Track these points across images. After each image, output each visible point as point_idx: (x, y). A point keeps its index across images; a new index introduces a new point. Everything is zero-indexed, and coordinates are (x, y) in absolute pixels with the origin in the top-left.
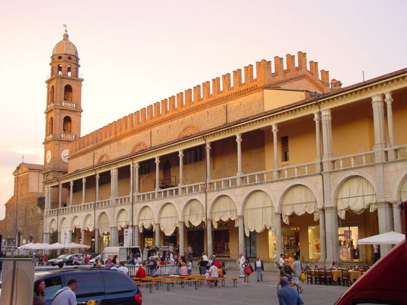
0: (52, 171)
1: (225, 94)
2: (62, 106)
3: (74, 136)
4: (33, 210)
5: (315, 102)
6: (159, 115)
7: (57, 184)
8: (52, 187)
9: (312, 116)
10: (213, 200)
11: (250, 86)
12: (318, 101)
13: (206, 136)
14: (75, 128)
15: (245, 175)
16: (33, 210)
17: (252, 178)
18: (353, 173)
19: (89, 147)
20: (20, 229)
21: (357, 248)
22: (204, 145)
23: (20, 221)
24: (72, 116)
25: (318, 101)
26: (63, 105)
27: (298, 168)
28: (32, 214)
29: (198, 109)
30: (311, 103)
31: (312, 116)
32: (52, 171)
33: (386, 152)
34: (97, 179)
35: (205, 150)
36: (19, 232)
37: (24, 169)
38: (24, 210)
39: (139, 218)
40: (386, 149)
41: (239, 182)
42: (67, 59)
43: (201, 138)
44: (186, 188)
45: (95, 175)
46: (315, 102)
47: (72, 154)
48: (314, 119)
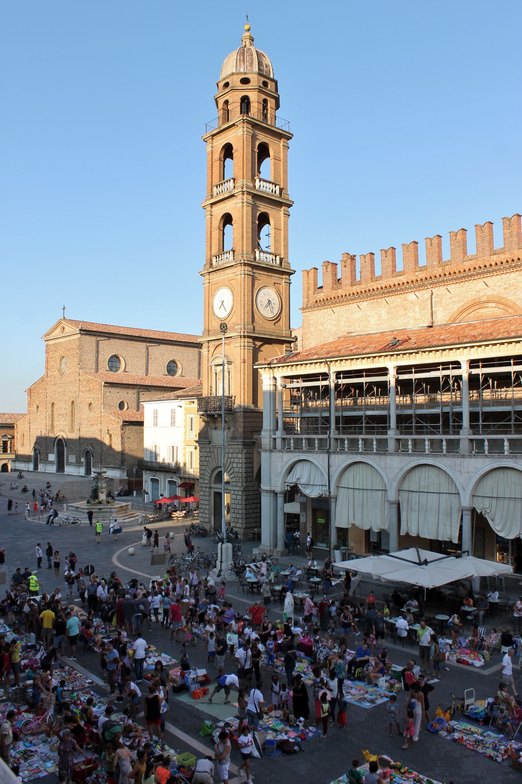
6: (373, 278)
23: (62, 422)
30: (404, 352)
38: (70, 403)
42: (262, 85)
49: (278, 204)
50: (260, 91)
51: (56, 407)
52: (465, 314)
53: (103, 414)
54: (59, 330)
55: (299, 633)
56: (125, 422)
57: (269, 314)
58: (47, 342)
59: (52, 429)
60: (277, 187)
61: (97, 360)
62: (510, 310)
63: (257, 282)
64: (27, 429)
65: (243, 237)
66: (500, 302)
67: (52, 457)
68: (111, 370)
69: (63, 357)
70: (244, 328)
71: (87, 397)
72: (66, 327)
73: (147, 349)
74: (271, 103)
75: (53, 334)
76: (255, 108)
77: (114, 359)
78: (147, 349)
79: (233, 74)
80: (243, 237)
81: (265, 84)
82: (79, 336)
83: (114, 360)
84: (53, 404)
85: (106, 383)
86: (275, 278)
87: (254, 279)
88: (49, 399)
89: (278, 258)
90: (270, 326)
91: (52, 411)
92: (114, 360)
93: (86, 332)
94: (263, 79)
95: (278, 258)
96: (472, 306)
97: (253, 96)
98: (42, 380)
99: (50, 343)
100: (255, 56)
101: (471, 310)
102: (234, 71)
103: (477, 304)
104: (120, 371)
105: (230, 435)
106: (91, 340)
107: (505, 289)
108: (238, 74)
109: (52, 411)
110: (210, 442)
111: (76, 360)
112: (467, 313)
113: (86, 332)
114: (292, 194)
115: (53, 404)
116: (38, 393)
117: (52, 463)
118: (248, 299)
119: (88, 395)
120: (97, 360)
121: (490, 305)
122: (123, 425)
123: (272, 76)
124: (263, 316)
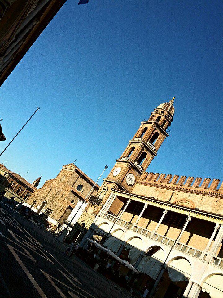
0: (115, 183)
2: (147, 143)
4: (63, 195)
5: (189, 210)
7: (127, 197)
8: (118, 197)
9: (215, 224)
15: (219, 258)
16: (63, 195)
19: (169, 185)
21: (30, 221)
22: (128, 199)
27: (190, 248)
29: (165, 188)
31: (215, 224)
32: (115, 183)
33: (206, 255)
35: (185, 221)
36: (45, 202)
37: (72, 167)
38: (57, 192)
39: (206, 280)
40: (207, 253)
44: (219, 260)
46: (189, 210)
47: (144, 181)
48: (144, 206)
49: (151, 153)
50: (165, 117)
51: (51, 191)
52: (179, 202)
53: (64, 200)
54: (69, 166)
55: (53, 225)
56: (69, 206)
57: (130, 183)
58: (63, 168)
59: (45, 198)
60: (154, 148)
61: (75, 183)
62: (192, 206)
63: (130, 171)
64: (37, 193)
65: (134, 155)
66: (191, 202)
67: (39, 207)
68: (77, 189)
69: (65, 176)
70: (118, 181)
71: (63, 192)
72: (72, 166)
73: (94, 190)
74: (167, 123)
75: (67, 167)
76: (160, 121)
77: (81, 186)
78: (94, 190)
79: (160, 108)
80: (134, 155)
81: (169, 116)
82: (74, 171)
83: (80, 187)
84: (51, 189)
85: (72, 190)
86: (137, 174)
87: (130, 169)
88: (51, 187)
89: (142, 168)
90: (127, 187)
91: (50, 191)
92: (80, 187)
93: (77, 171)
94: (168, 114)
95: (142, 168)
96: (183, 200)
97: (163, 118)
98: (53, 179)
99: (64, 169)
100: (170, 106)
102: (161, 108)
103: (185, 201)
104: (80, 191)
105: (94, 212)
106: (76, 175)
107: (194, 199)
108: (161, 109)
109: (50, 191)
110: (87, 212)
111: (68, 178)
113: (77, 171)
114: (158, 153)
115: (51, 189)
116: (49, 183)
118: (124, 174)
119: (64, 192)
120: (75, 183)
121: (188, 202)
122: (68, 207)
123: (172, 115)
124: (126, 182)
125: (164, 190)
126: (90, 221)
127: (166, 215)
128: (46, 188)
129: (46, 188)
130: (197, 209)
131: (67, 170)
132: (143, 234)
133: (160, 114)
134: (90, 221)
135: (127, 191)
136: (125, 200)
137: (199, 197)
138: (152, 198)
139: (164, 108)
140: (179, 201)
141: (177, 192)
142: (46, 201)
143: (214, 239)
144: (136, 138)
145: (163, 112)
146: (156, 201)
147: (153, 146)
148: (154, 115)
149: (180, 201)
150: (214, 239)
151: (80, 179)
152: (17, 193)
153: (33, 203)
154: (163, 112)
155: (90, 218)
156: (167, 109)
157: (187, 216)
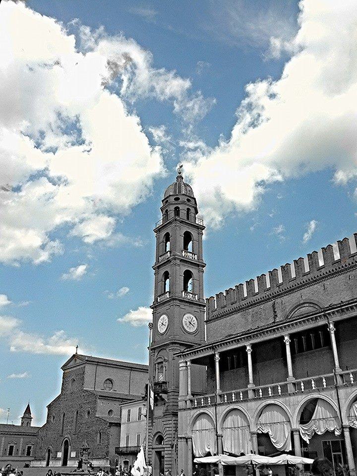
1: (248, 300)
3: (196, 296)
8: (193, 362)
10: (224, 413)
11: (331, 268)
12: (326, 312)
13: (329, 314)
14: (196, 286)
16: (89, 413)
17: (308, 384)
18: (202, 411)
20: (67, 436)
24: (194, 270)
25: (326, 312)
26: (184, 255)
28: (87, 417)
34: (288, 343)
36: (67, 441)
38: (76, 413)
41: (251, 395)
43: (210, 348)
45: (214, 355)
48: (284, 341)
52: (293, 313)
60: (196, 256)
84: (64, 415)
86: (195, 308)
95: (196, 296)
96: (296, 307)
101: (296, 309)
105: (165, 409)
107: (313, 294)
112: (294, 311)
115: (64, 415)
117: (59, 459)
121: (305, 305)
125: (255, 309)
126: (168, 426)
127: (290, 343)
128: (54, 418)
129: (54, 418)
130: (331, 307)
131: (72, 369)
132: (276, 395)
133: (174, 204)
134: (168, 426)
135: (200, 345)
136: (209, 361)
137: (317, 287)
138: (330, 306)
139: (175, 191)
140: (291, 312)
141: (278, 300)
142: (66, 439)
143: (139, 436)
144: (161, 256)
145: (177, 199)
146: (261, 331)
147: (191, 253)
148: (167, 210)
149: (293, 310)
150: (139, 436)
151: (101, 369)
152: (10, 454)
153: (47, 454)
154: (177, 199)
155: (165, 423)
156: (180, 192)
157: (325, 327)
